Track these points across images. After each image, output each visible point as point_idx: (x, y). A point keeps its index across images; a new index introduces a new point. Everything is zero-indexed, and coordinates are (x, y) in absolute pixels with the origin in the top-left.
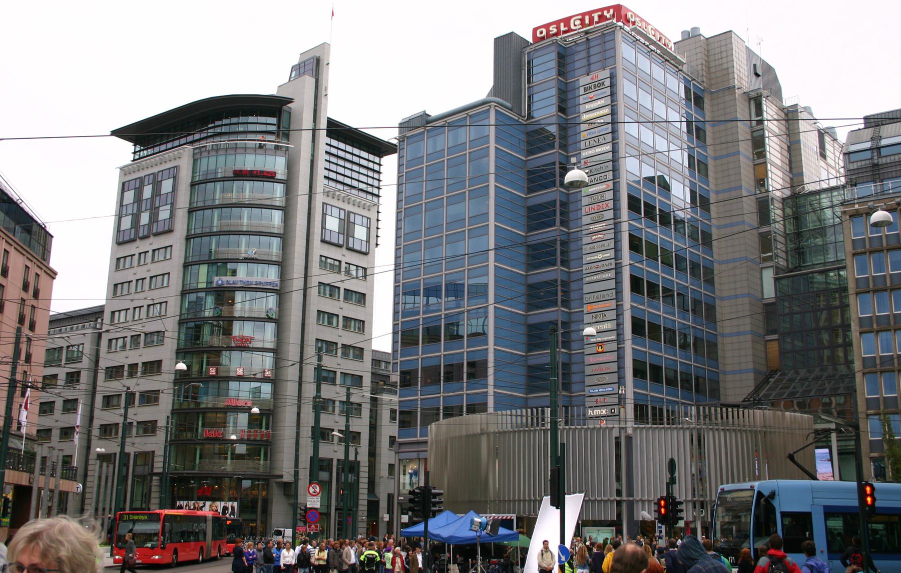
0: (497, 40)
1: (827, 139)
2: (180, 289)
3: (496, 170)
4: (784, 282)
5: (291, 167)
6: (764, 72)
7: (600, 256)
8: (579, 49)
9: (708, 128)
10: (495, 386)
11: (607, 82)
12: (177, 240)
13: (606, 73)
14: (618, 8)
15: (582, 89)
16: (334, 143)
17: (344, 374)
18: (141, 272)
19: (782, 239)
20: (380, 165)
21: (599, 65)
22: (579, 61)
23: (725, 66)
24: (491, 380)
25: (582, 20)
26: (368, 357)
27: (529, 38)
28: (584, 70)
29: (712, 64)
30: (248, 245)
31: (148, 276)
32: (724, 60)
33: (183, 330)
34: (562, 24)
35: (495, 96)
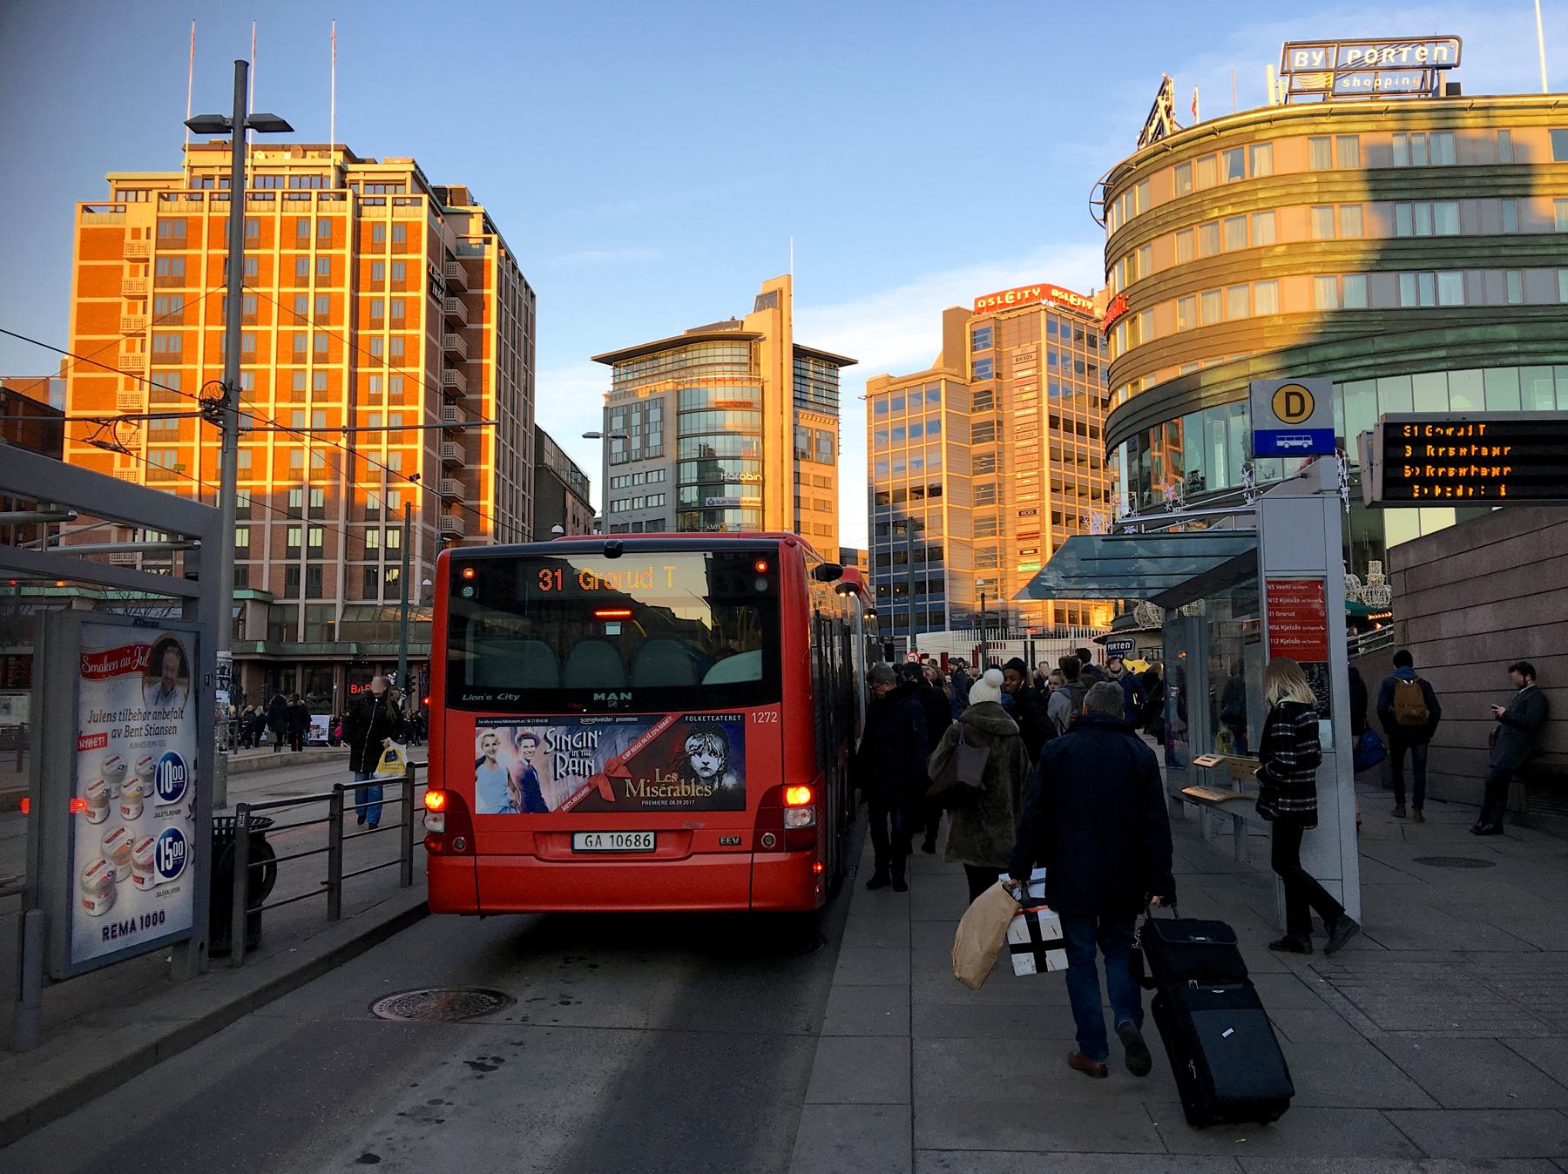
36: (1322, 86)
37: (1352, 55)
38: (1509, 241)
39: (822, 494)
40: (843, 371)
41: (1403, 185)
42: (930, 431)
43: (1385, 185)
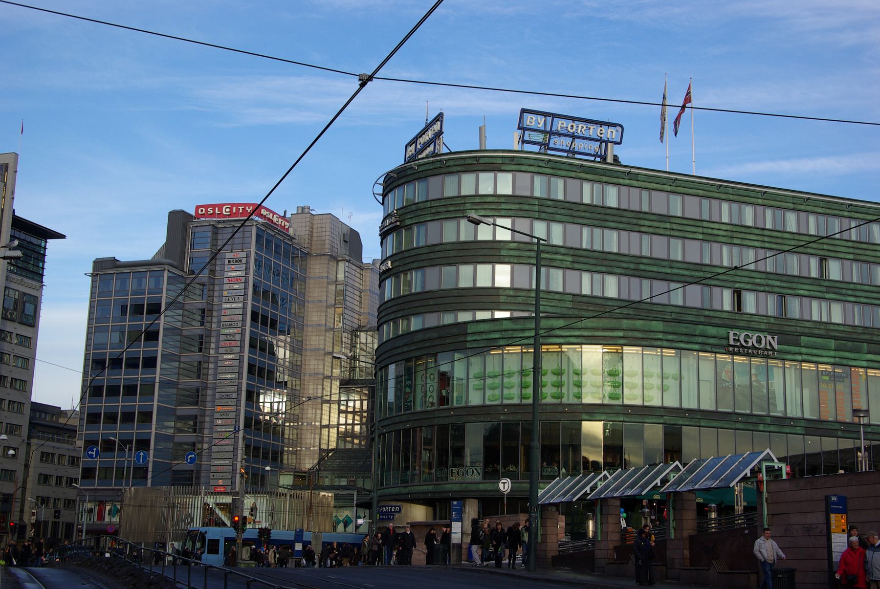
7: (229, 376)
10: (154, 456)
11: (244, 261)
13: (244, 254)
15: (227, 261)
27: (193, 213)
35: (166, 257)
36: (541, 141)
37: (560, 124)
38: (645, 261)
39: (21, 351)
40: (51, 244)
41: (588, 215)
42: (150, 312)
43: (577, 214)
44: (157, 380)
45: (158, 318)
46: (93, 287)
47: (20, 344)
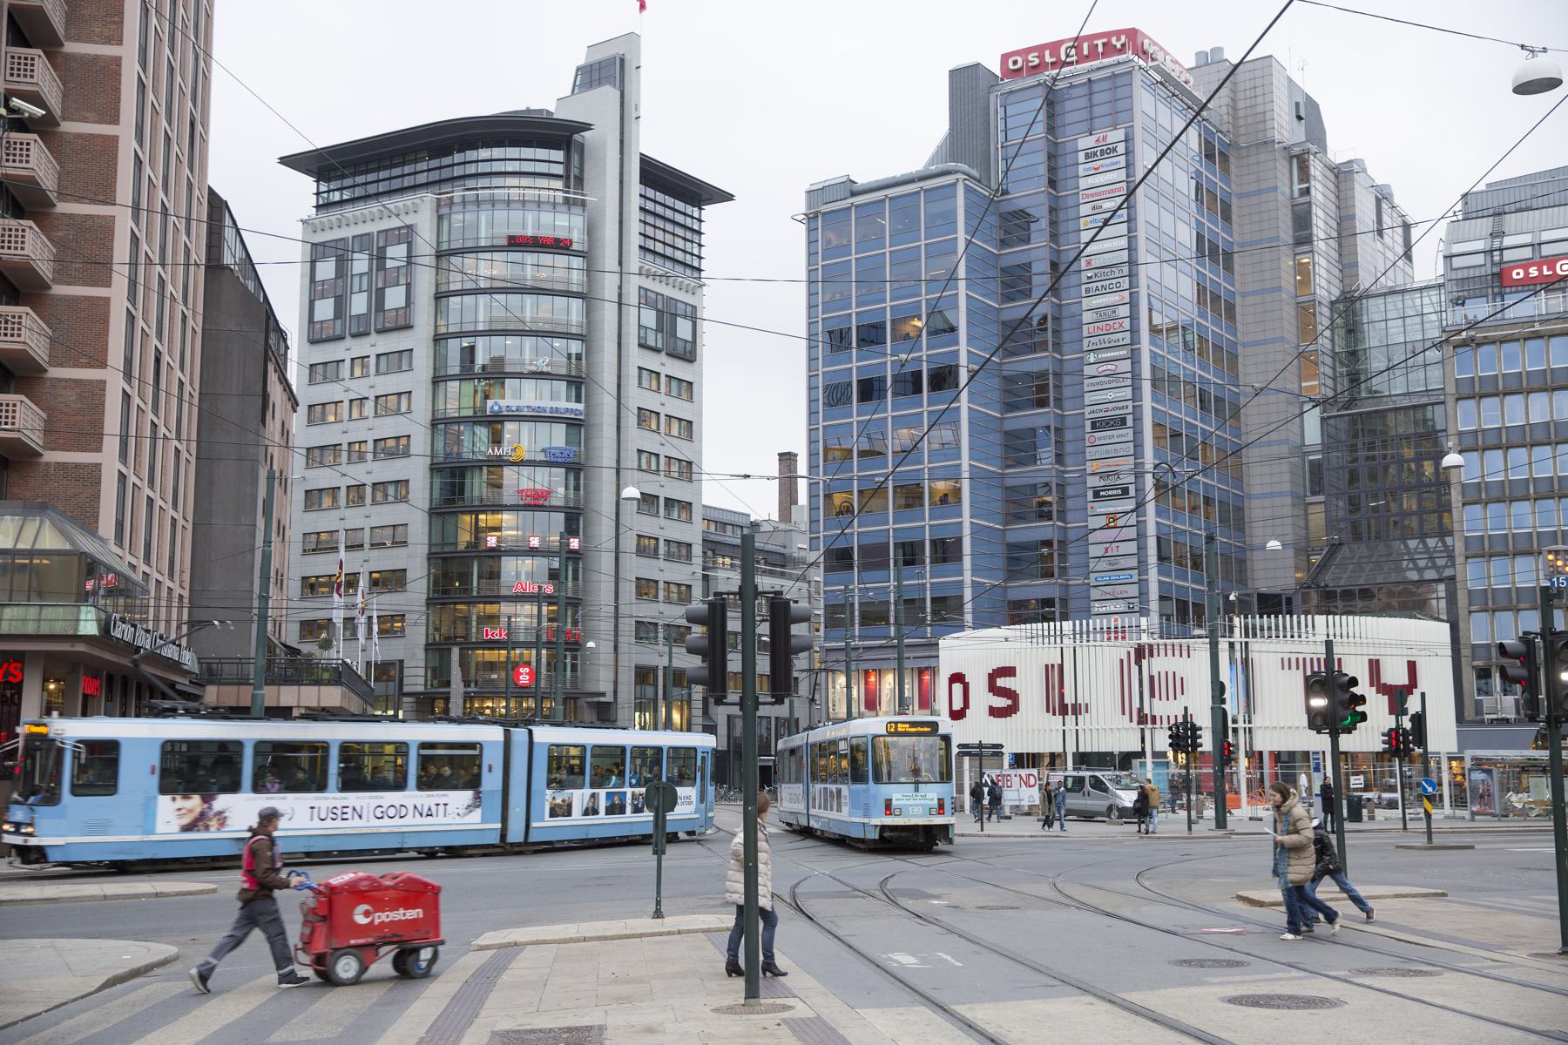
0: (954, 74)
1: (1385, 206)
2: (430, 417)
3: (967, 273)
4: (1332, 422)
5: (591, 230)
6: (1307, 113)
8: (1075, 93)
9: (1235, 202)
10: (974, 572)
11: (1121, 148)
12: (418, 340)
13: (1118, 135)
14: (1132, 34)
15: (1081, 156)
16: (650, 193)
17: (668, 541)
18: (360, 388)
19: (1329, 361)
20: (700, 221)
21: (1108, 120)
22: (1073, 110)
23: (1260, 109)
24: (967, 562)
25: (1078, 48)
26: (697, 515)
28: (1085, 126)
29: (1241, 105)
30: (537, 352)
31: (372, 394)
32: (1260, 100)
33: (437, 481)
34: (1047, 53)
44: (967, 531)
45: (956, 398)
46: (811, 242)
47: (669, 557)
